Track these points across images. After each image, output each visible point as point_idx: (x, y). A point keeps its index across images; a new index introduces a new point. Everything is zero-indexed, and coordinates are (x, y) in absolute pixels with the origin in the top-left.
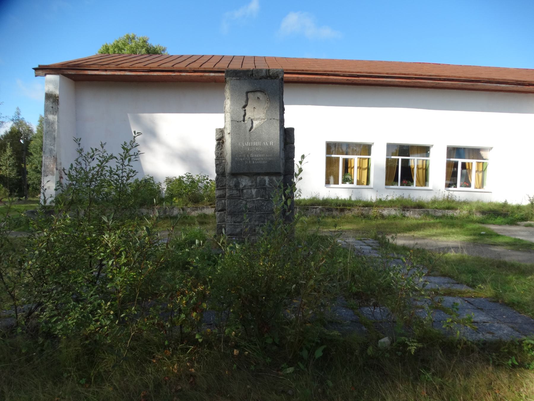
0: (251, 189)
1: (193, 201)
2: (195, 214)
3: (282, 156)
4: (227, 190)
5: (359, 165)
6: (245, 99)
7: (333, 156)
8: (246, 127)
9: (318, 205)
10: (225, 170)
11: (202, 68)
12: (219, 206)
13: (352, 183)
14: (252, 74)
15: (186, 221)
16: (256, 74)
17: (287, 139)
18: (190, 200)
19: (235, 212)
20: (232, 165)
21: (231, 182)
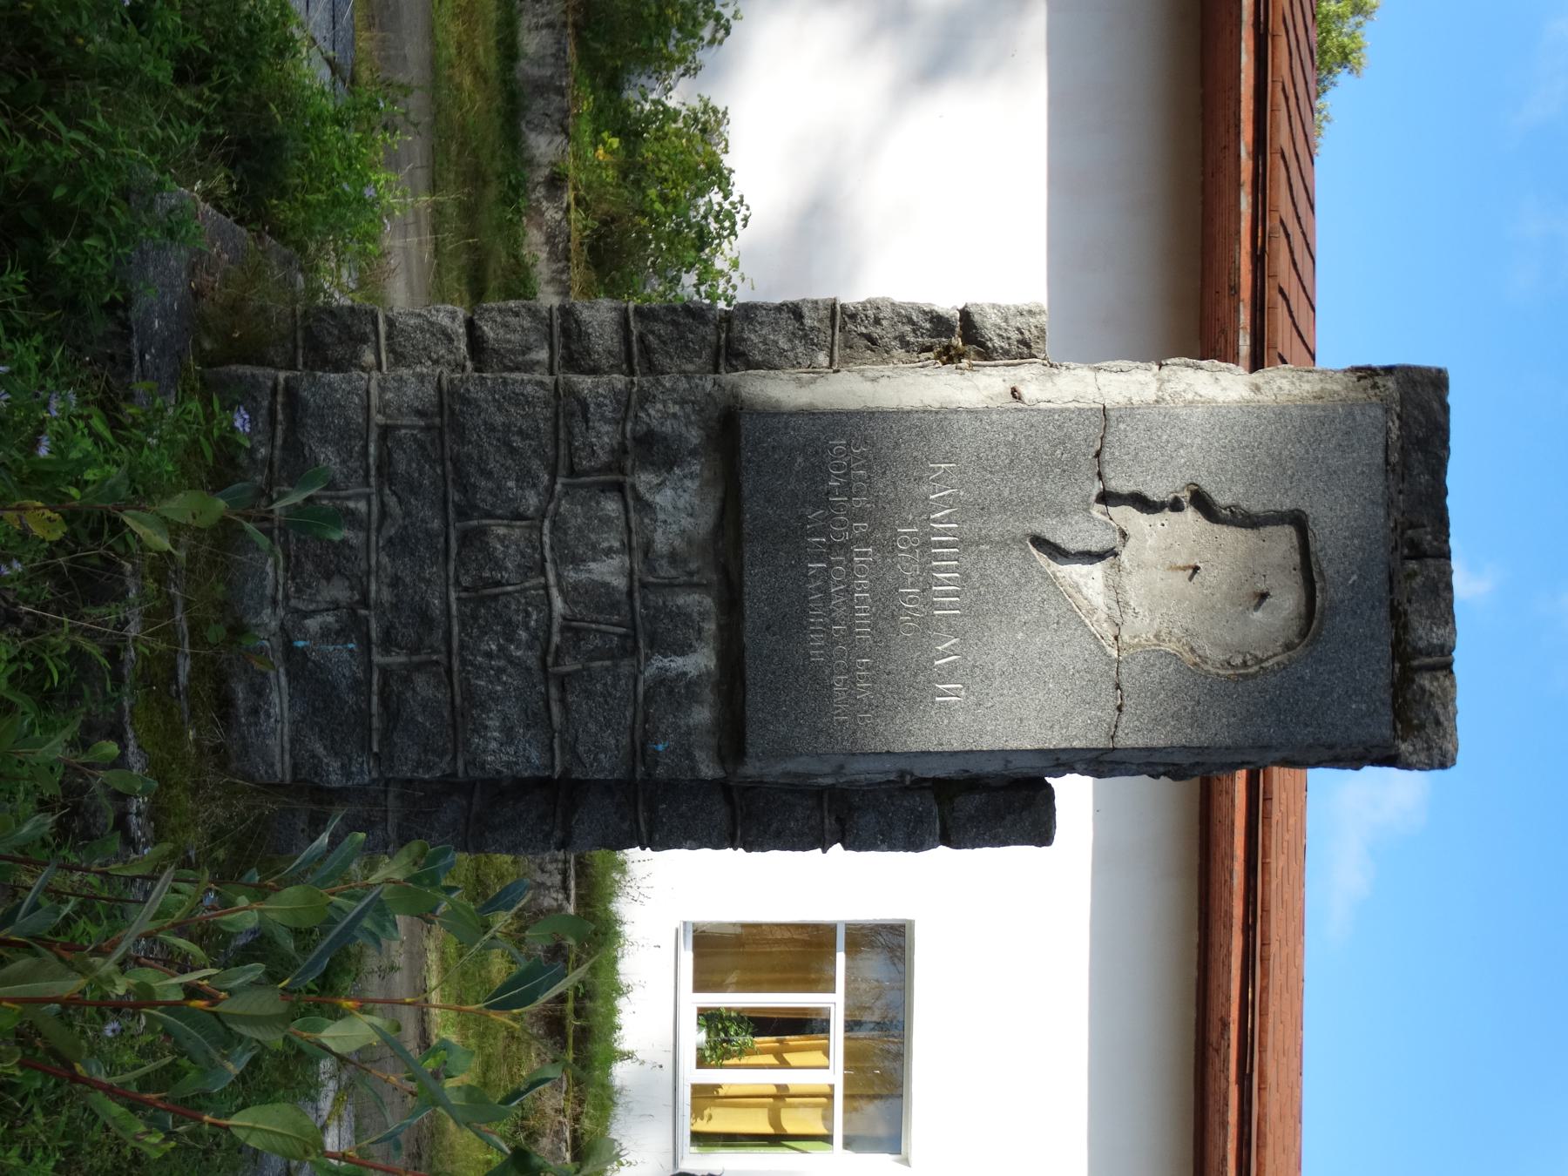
0: (627, 548)
1: (600, 237)
2: (534, 244)
3: (860, 771)
4: (619, 381)
5: (792, 1090)
6: (1256, 506)
7: (841, 957)
8: (1061, 512)
9: (579, 897)
10: (758, 366)
11: (1271, 294)
12: (506, 325)
13: (701, 1063)
14: (1417, 553)
15: (492, 193)
16: (1419, 579)
17: (978, 799)
18: (604, 223)
19: (462, 439)
20: (792, 414)
21: (674, 409)
